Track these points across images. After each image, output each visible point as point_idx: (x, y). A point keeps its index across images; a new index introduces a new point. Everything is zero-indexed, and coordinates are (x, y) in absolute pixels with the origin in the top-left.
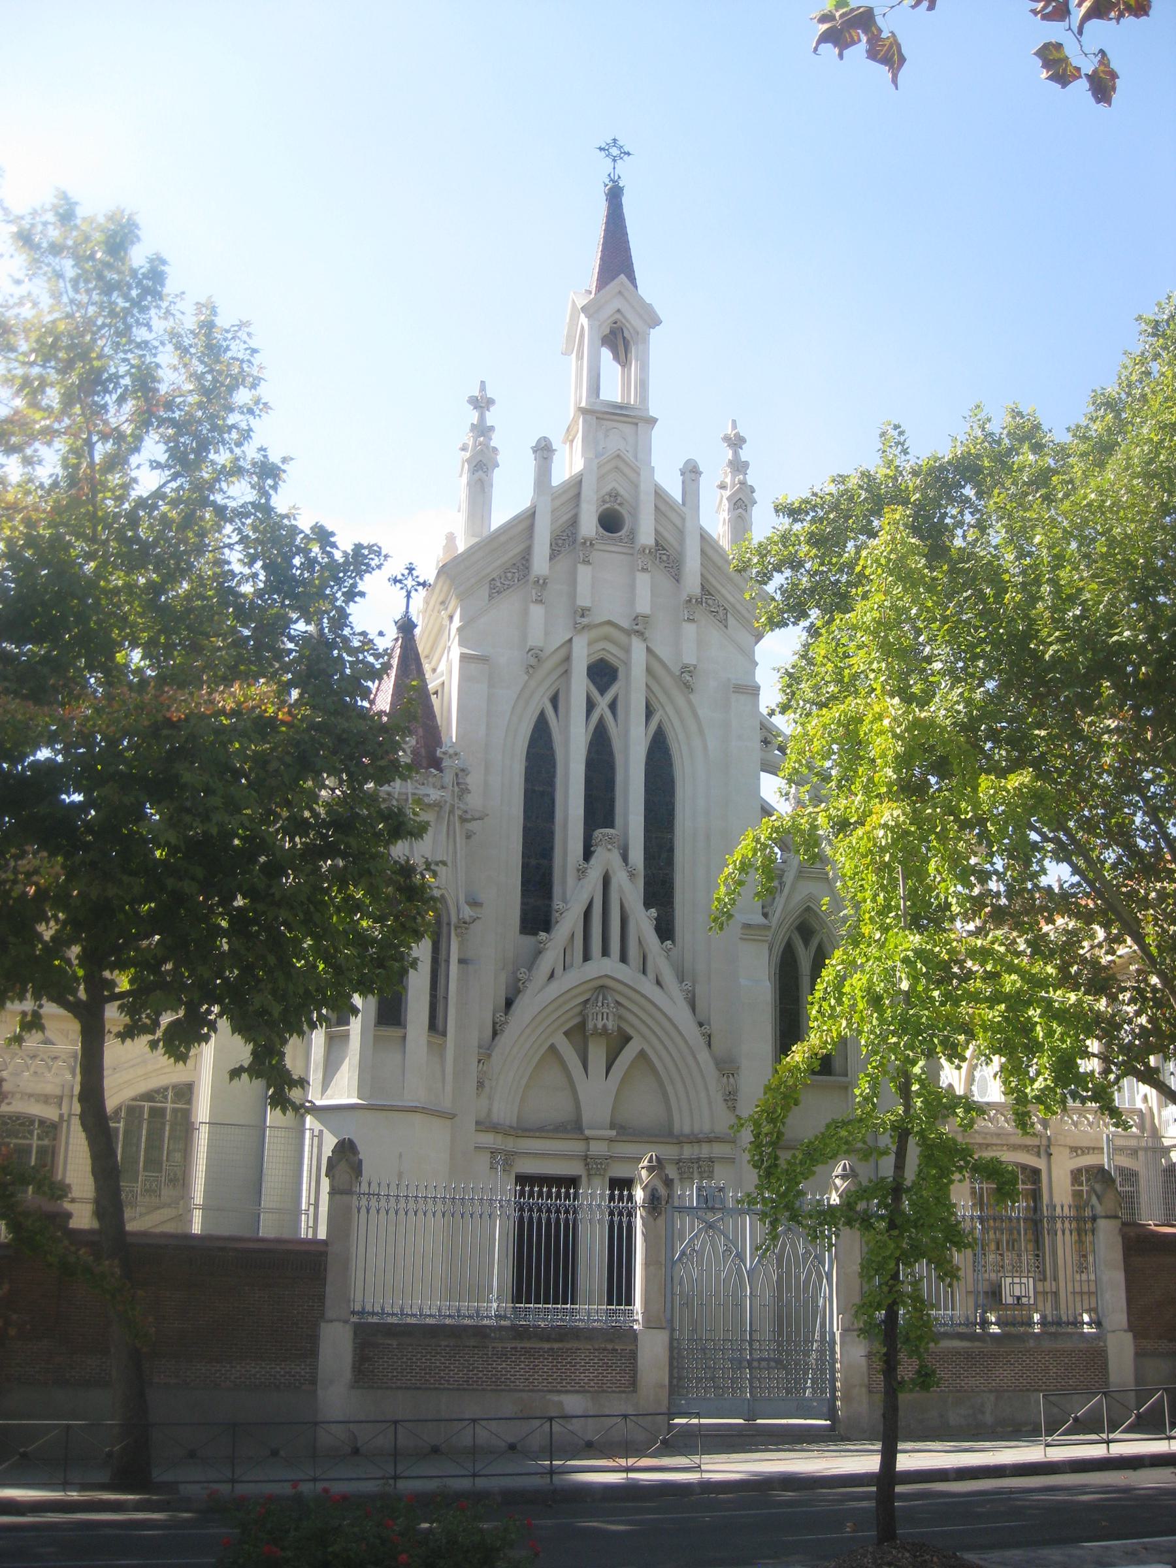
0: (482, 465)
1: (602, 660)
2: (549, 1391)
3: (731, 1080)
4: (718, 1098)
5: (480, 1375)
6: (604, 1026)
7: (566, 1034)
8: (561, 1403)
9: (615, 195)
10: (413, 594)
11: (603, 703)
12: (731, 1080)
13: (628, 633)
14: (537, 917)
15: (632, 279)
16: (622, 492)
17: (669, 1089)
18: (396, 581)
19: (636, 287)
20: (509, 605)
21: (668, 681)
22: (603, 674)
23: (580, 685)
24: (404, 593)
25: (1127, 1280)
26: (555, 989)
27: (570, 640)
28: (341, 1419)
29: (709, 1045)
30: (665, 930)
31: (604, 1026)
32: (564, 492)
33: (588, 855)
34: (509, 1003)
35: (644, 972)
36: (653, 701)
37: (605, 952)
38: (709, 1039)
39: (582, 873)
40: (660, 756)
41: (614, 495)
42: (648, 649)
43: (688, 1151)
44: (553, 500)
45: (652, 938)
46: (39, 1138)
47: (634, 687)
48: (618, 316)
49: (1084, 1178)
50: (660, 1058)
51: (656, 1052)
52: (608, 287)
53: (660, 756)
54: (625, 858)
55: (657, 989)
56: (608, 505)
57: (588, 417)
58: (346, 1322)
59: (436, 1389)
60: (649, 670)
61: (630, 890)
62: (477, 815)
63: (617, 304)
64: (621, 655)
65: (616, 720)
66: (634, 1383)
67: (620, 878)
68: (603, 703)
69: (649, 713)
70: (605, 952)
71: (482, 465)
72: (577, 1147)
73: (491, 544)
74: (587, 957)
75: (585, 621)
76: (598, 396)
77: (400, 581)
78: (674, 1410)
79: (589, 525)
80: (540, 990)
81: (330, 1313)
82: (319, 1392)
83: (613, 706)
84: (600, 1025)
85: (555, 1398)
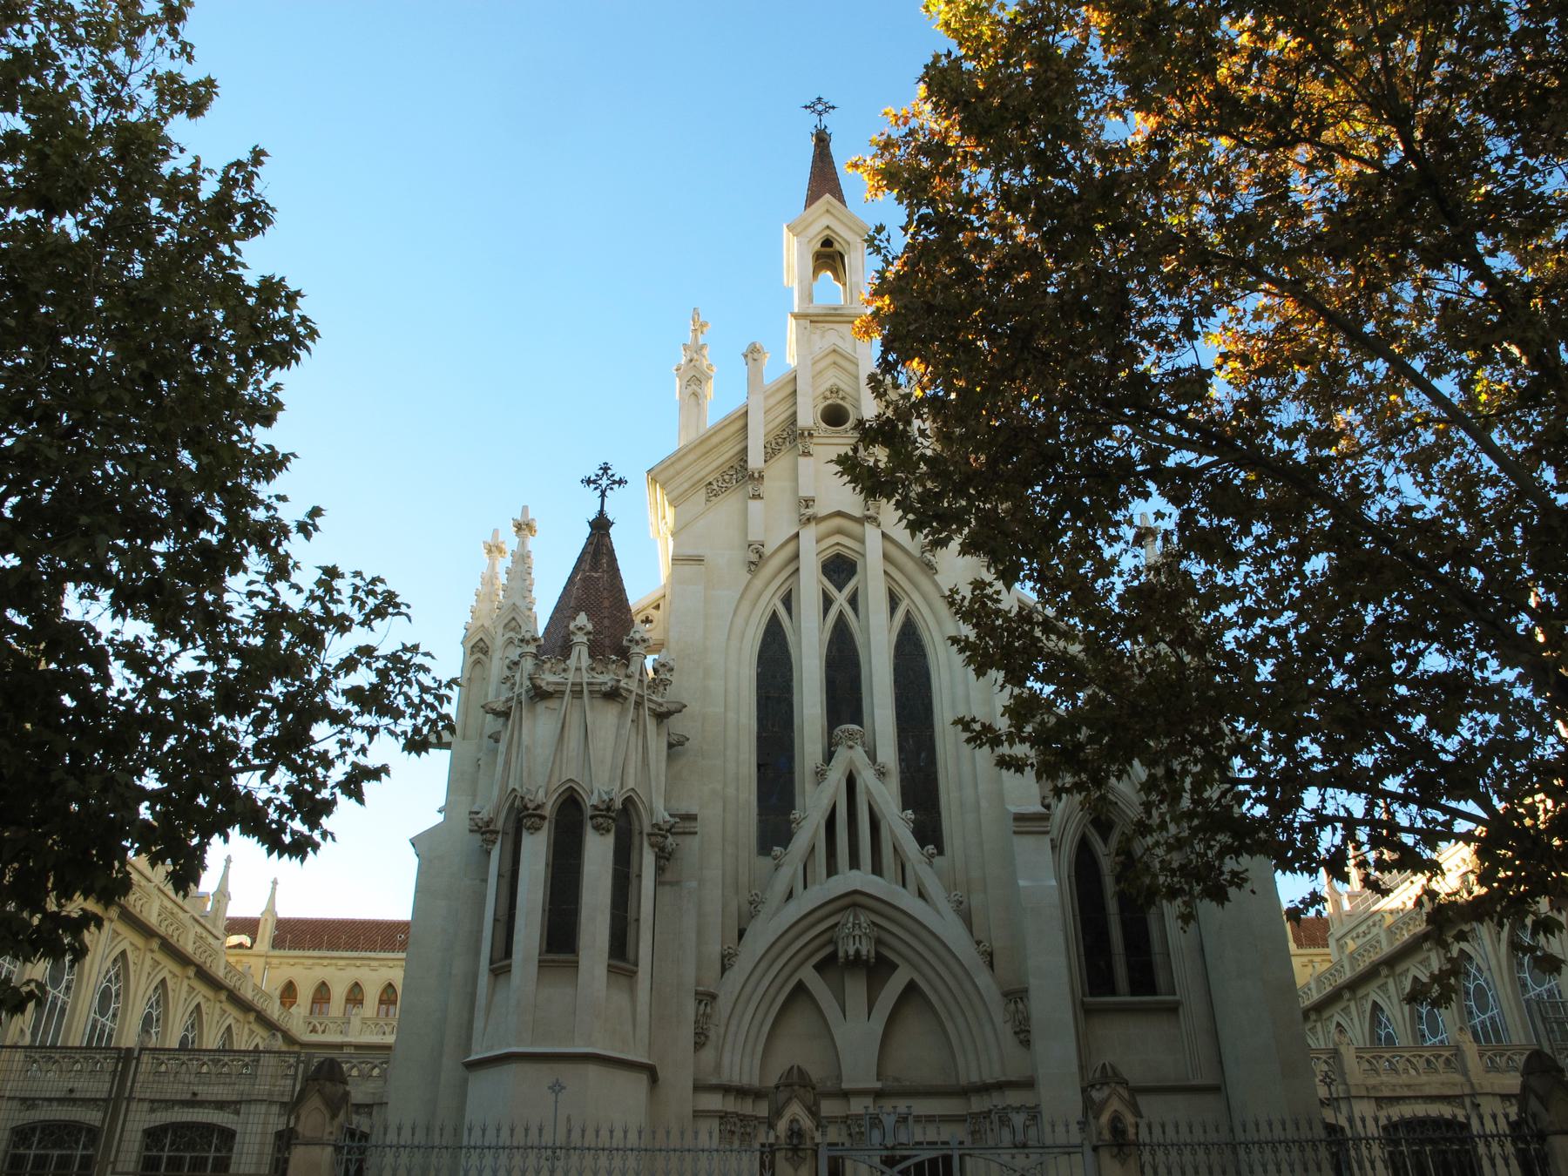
0: (695, 379)
1: (838, 555)
3: (1020, 1006)
4: (1007, 1031)
6: (858, 952)
7: (818, 967)
9: (822, 140)
10: (608, 492)
11: (841, 599)
12: (1020, 1006)
13: (861, 521)
15: (840, 198)
16: (843, 386)
17: (949, 1026)
18: (589, 482)
19: (843, 202)
20: (729, 505)
21: (910, 566)
23: (811, 582)
24: (598, 492)
25: (622, 591)
26: (794, 911)
27: (797, 535)
29: (991, 965)
30: (929, 833)
31: (858, 952)
32: (778, 390)
33: (829, 756)
34: (741, 934)
35: (904, 885)
36: (897, 589)
37: (854, 863)
38: (990, 958)
39: (820, 775)
41: (835, 391)
42: (884, 535)
43: (978, 1104)
44: (766, 398)
45: (910, 845)
46: (85, 1148)
48: (827, 232)
49: (168, 1141)
50: (936, 991)
51: (928, 981)
52: (818, 203)
54: (872, 755)
55: (920, 902)
57: (802, 321)
60: (886, 557)
61: (886, 795)
62: (673, 707)
63: (826, 220)
67: (867, 777)
68: (841, 599)
69: (894, 602)
70: (854, 863)
71: (695, 379)
73: (703, 446)
74: (832, 870)
75: (810, 511)
76: (811, 301)
77: (594, 482)
79: (808, 416)
80: (774, 915)
83: (853, 601)
84: (851, 952)
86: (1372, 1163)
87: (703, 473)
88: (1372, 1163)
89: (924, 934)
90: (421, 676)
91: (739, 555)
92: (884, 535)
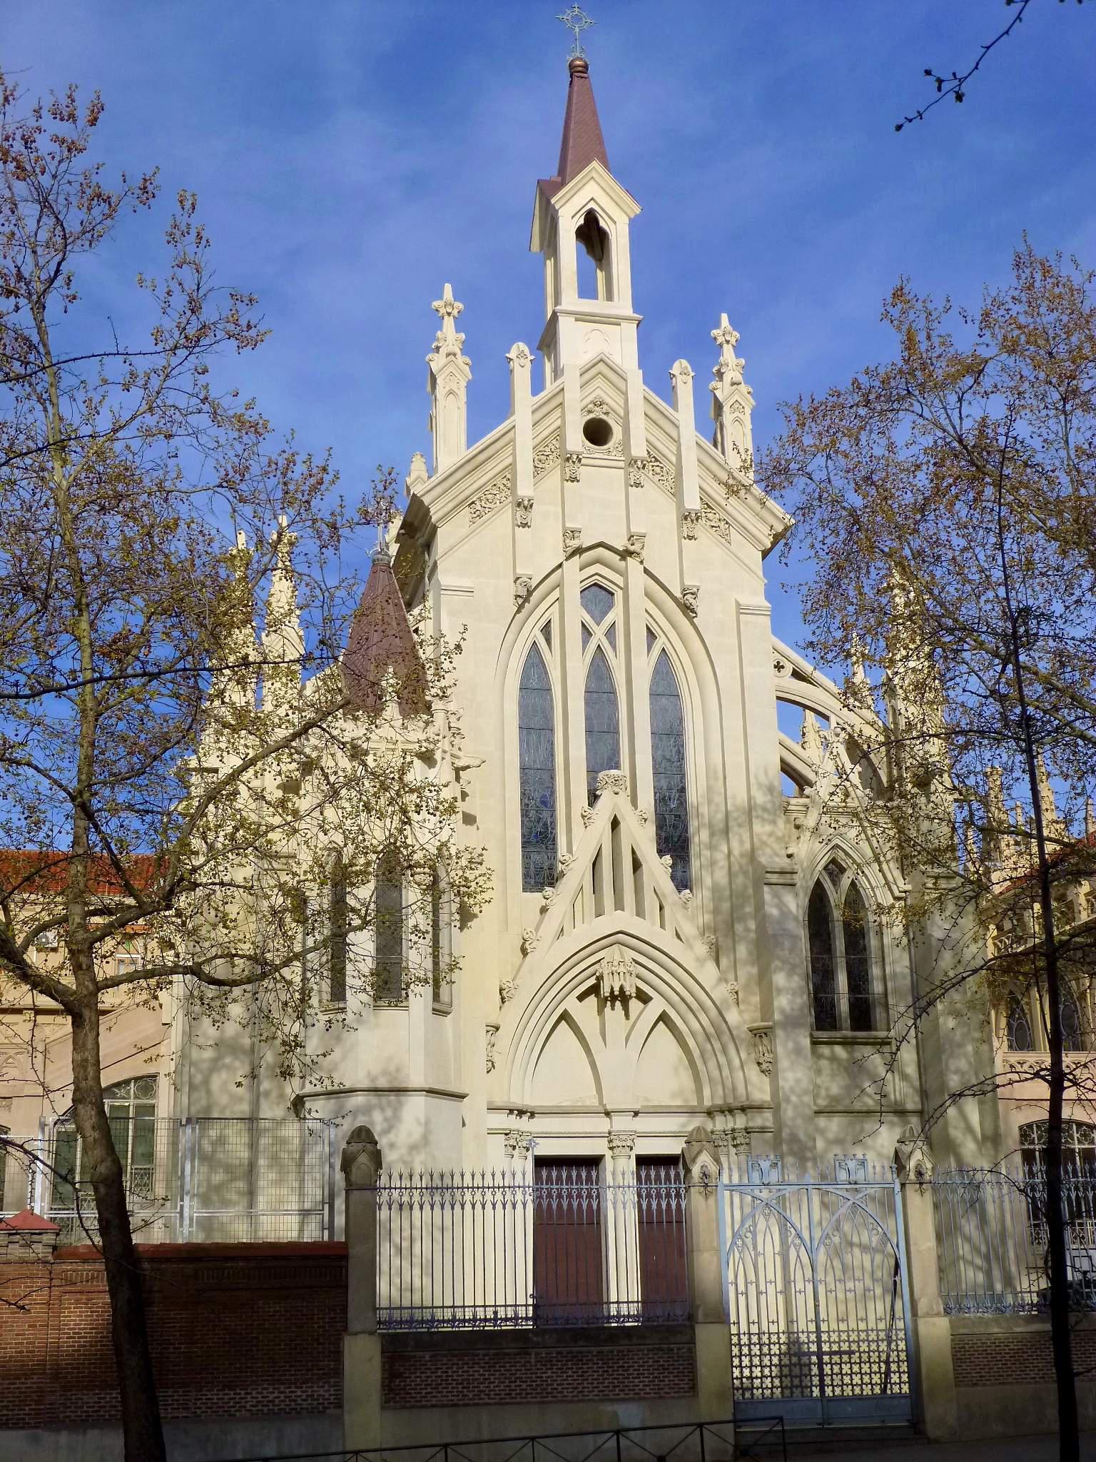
2: (602, 1400)
5: (524, 1386)
8: (615, 1414)
11: (599, 632)
14: (541, 874)
16: (608, 400)
22: (598, 596)
28: (376, 1447)
33: (593, 798)
35: (662, 926)
37: (619, 905)
40: (665, 687)
45: (668, 886)
47: (637, 603)
53: (665, 687)
54: (634, 802)
56: (592, 416)
58: (372, 1333)
59: (475, 1405)
64: (619, 580)
65: (614, 648)
66: (694, 1387)
68: (599, 632)
69: (651, 635)
70: (619, 905)
72: (602, 1124)
78: (740, 1416)
81: (354, 1325)
82: (346, 1417)
85: (609, 1408)
86: (624, 1204)
87: (467, 493)
88: (624, 1204)
89: (680, 972)
90: (354, 869)
91: (510, 590)
92: (646, 571)
